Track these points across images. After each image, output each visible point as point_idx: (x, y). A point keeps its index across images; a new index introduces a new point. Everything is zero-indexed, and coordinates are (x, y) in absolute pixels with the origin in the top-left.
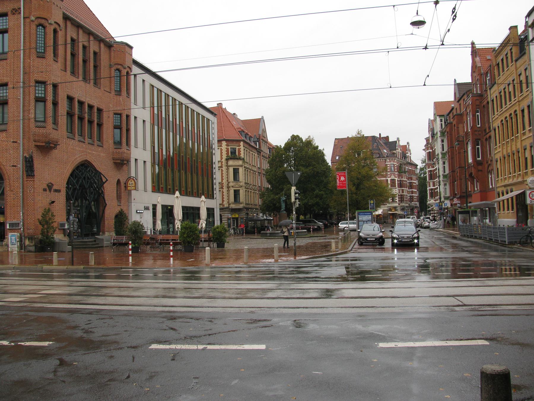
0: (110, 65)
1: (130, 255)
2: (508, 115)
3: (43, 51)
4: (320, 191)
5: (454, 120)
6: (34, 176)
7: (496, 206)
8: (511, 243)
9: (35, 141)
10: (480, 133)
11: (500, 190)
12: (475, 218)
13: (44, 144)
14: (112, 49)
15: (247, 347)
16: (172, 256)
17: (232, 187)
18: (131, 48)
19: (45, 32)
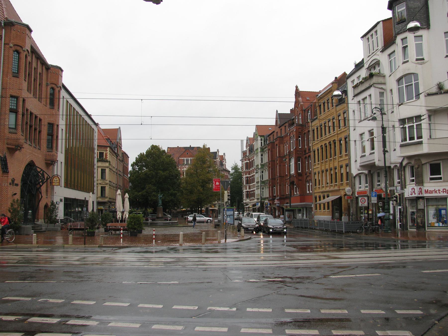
0: (47, 84)
1: (121, 238)
2: (327, 142)
3: (16, 72)
4: (174, 190)
5: (276, 141)
6: (8, 172)
7: (313, 206)
8: (347, 232)
9: (7, 144)
10: (301, 152)
11: (318, 195)
12: (300, 215)
13: (14, 147)
14: (49, 71)
15: (428, 271)
16: (154, 239)
17: (100, 184)
18: (62, 71)
19: (19, 57)
